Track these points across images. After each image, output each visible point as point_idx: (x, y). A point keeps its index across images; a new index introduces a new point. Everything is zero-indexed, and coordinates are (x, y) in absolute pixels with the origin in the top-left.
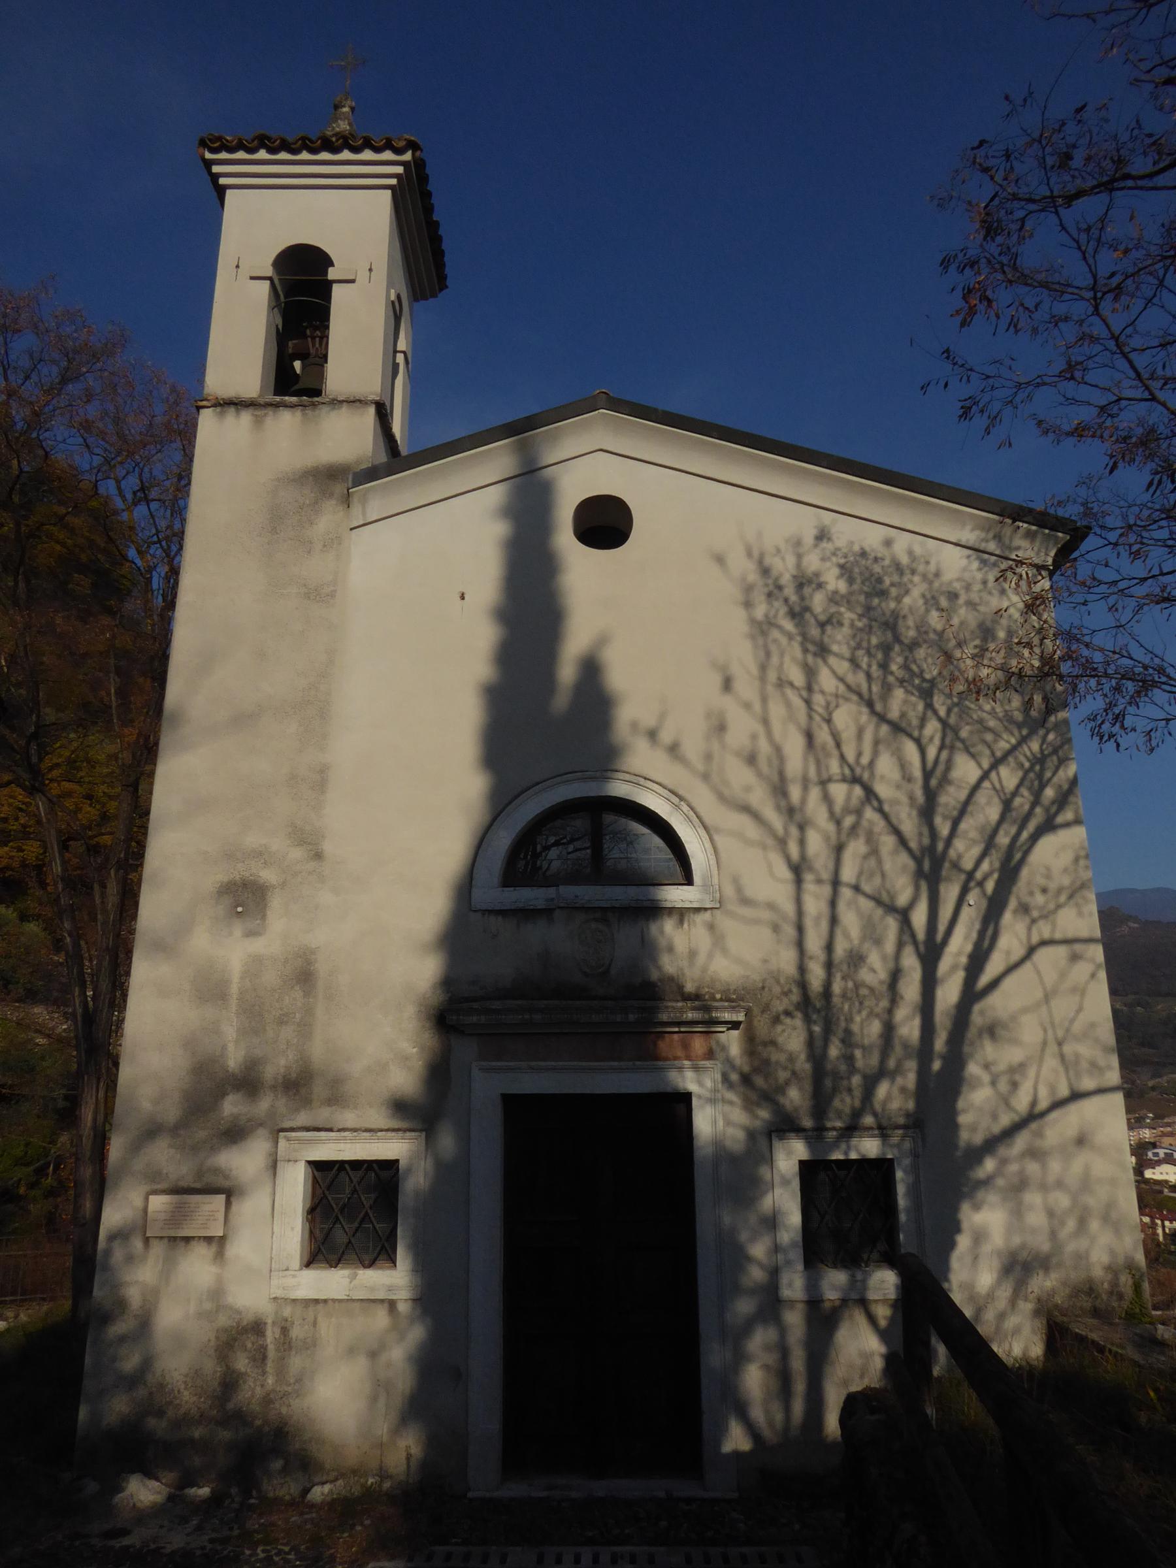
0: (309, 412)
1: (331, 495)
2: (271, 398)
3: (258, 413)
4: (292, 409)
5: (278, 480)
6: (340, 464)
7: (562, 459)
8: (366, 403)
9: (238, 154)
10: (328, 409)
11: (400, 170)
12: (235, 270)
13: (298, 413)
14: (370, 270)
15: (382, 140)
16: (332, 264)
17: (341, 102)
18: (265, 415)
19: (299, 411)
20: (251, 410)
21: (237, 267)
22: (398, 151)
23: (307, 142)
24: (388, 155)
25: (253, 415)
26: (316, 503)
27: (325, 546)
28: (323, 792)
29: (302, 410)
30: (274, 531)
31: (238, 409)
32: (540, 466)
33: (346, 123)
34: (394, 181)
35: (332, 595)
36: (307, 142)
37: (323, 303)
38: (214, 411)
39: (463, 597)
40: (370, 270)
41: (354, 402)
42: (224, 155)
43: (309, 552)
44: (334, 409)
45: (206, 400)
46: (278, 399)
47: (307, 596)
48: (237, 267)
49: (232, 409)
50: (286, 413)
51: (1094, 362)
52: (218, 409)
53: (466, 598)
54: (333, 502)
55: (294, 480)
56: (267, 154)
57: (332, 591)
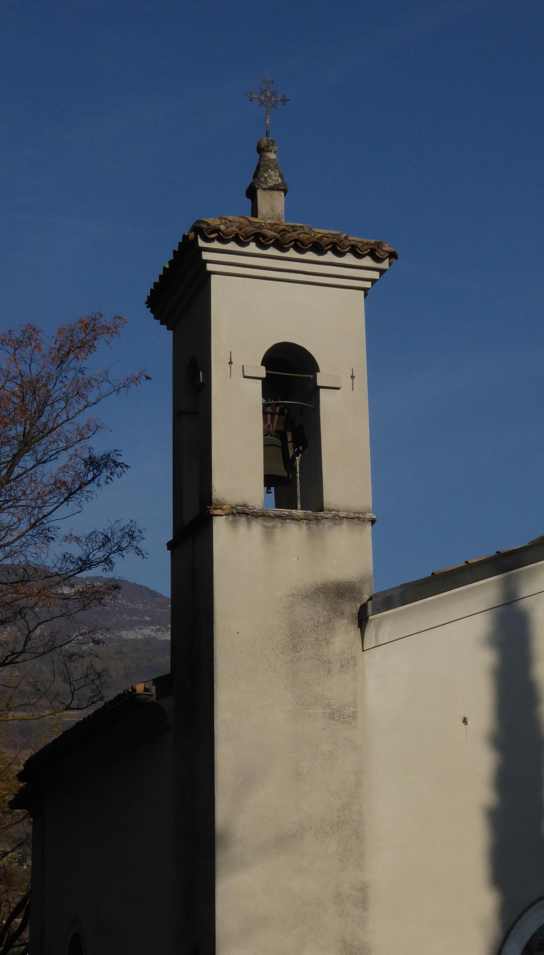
0: (313, 526)
1: (342, 614)
2: (274, 510)
3: (269, 524)
4: (298, 522)
5: (293, 596)
6: (346, 582)
7: (480, 613)
8: (364, 521)
9: (229, 244)
10: (330, 524)
11: (376, 275)
12: (229, 366)
13: (304, 525)
14: (353, 377)
15: (367, 250)
16: (319, 371)
17: (268, 147)
18: (274, 527)
19: (304, 524)
20: (260, 520)
21: (231, 363)
22: (378, 260)
23: (299, 243)
24: (367, 261)
25: (263, 525)
26: (330, 621)
27: (342, 666)
28: (365, 909)
29: (307, 524)
30: (295, 649)
31: (248, 518)
32: (517, 599)
33: (278, 174)
34: (368, 285)
35: (354, 715)
36: (299, 243)
37: (305, 404)
38: (227, 519)
39: (465, 721)
40: (353, 377)
41: (353, 518)
42: (216, 245)
43: (329, 672)
44: (335, 524)
45: (221, 508)
46: (276, 509)
47: (332, 716)
48: (231, 363)
49: (243, 519)
50: (336, 529)
51: (97, 562)
52: (231, 518)
53: (468, 723)
54: (345, 621)
55: (307, 597)
56: (257, 248)
57: (353, 713)
